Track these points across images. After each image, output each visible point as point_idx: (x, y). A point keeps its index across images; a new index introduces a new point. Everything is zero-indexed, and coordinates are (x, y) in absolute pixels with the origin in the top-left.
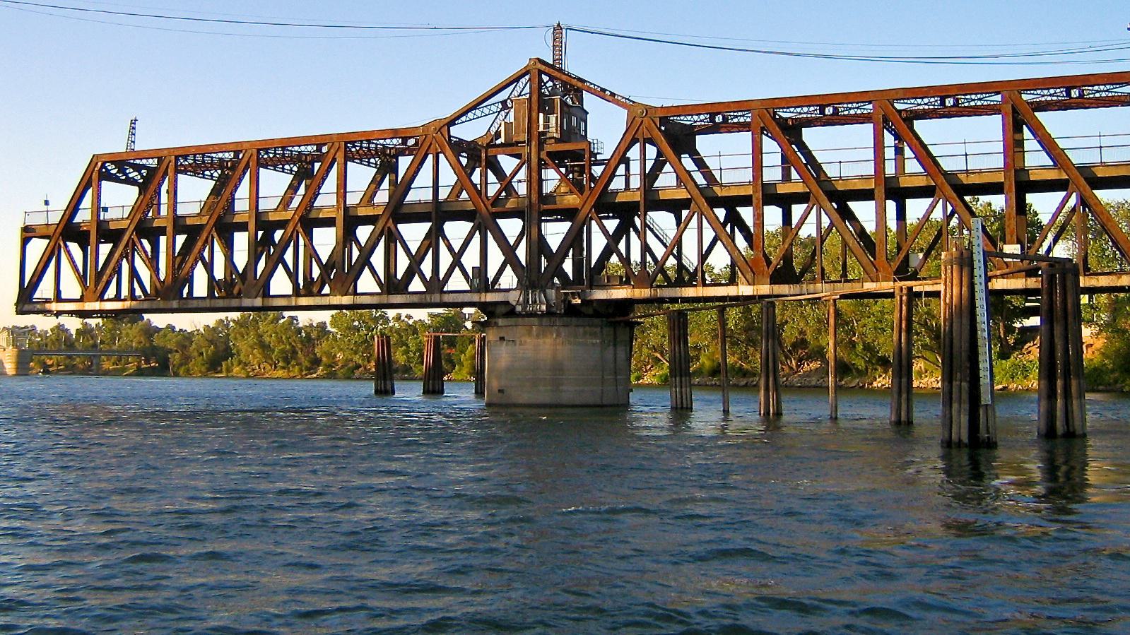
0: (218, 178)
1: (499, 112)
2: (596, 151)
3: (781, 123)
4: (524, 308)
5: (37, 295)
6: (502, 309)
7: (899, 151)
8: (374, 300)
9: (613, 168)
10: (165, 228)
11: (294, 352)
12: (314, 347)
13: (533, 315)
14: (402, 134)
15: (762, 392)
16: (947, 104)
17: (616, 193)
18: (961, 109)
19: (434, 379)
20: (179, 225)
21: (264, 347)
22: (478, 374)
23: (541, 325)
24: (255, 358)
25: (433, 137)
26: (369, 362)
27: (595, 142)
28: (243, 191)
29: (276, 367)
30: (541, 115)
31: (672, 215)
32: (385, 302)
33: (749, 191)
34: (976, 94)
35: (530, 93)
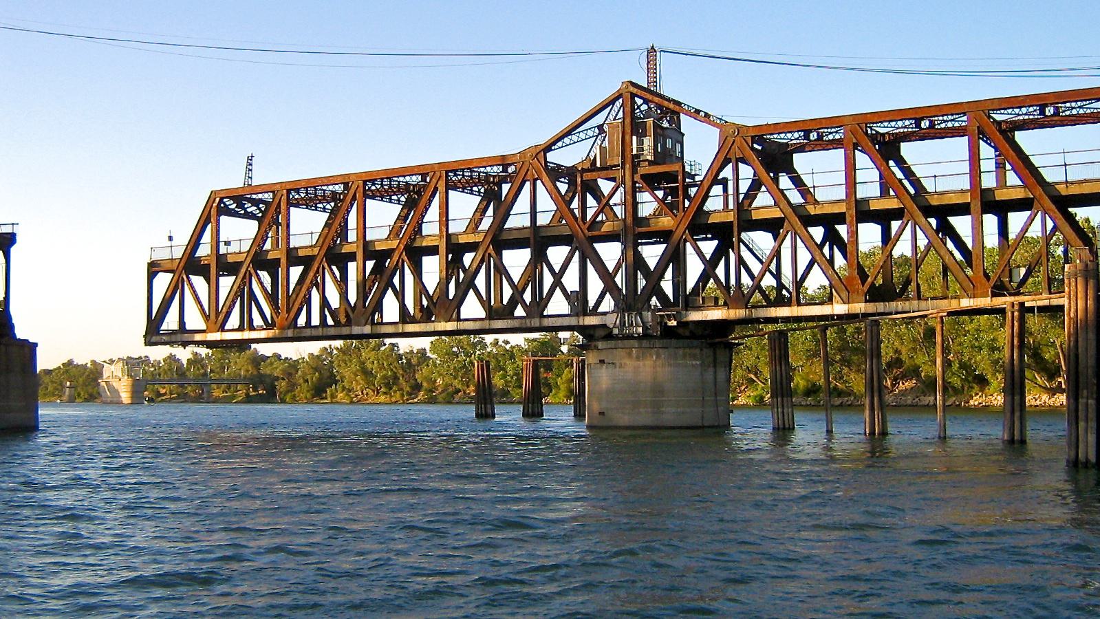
0: (405, 202)
1: (597, 136)
2: (693, 173)
3: (880, 140)
4: (621, 330)
5: (164, 327)
6: (602, 333)
7: (1000, 166)
8: (477, 325)
9: (706, 189)
10: (437, 247)
11: (396, 378)
12: (414, 372)
13: (630, 337)
14: (504, 161)
15: (867, 412)
16: (1047, 113)
17: (267, 251)
18: (1063, 118)
19: (533, 403)
20: (369, 251)
21: (367, 373)
22: (578, 398)
23: (640, 347)
24: (358, 384)
25: (530, 163)
26: (468, 387)
27: (693, 163)
28: (433, 213)
29: (378, 393)
30: (634, 138)
31: (770, 234)
32: (487, 327)
33: (842, 208)
34: (1076, 101)
35: (623, 118)
